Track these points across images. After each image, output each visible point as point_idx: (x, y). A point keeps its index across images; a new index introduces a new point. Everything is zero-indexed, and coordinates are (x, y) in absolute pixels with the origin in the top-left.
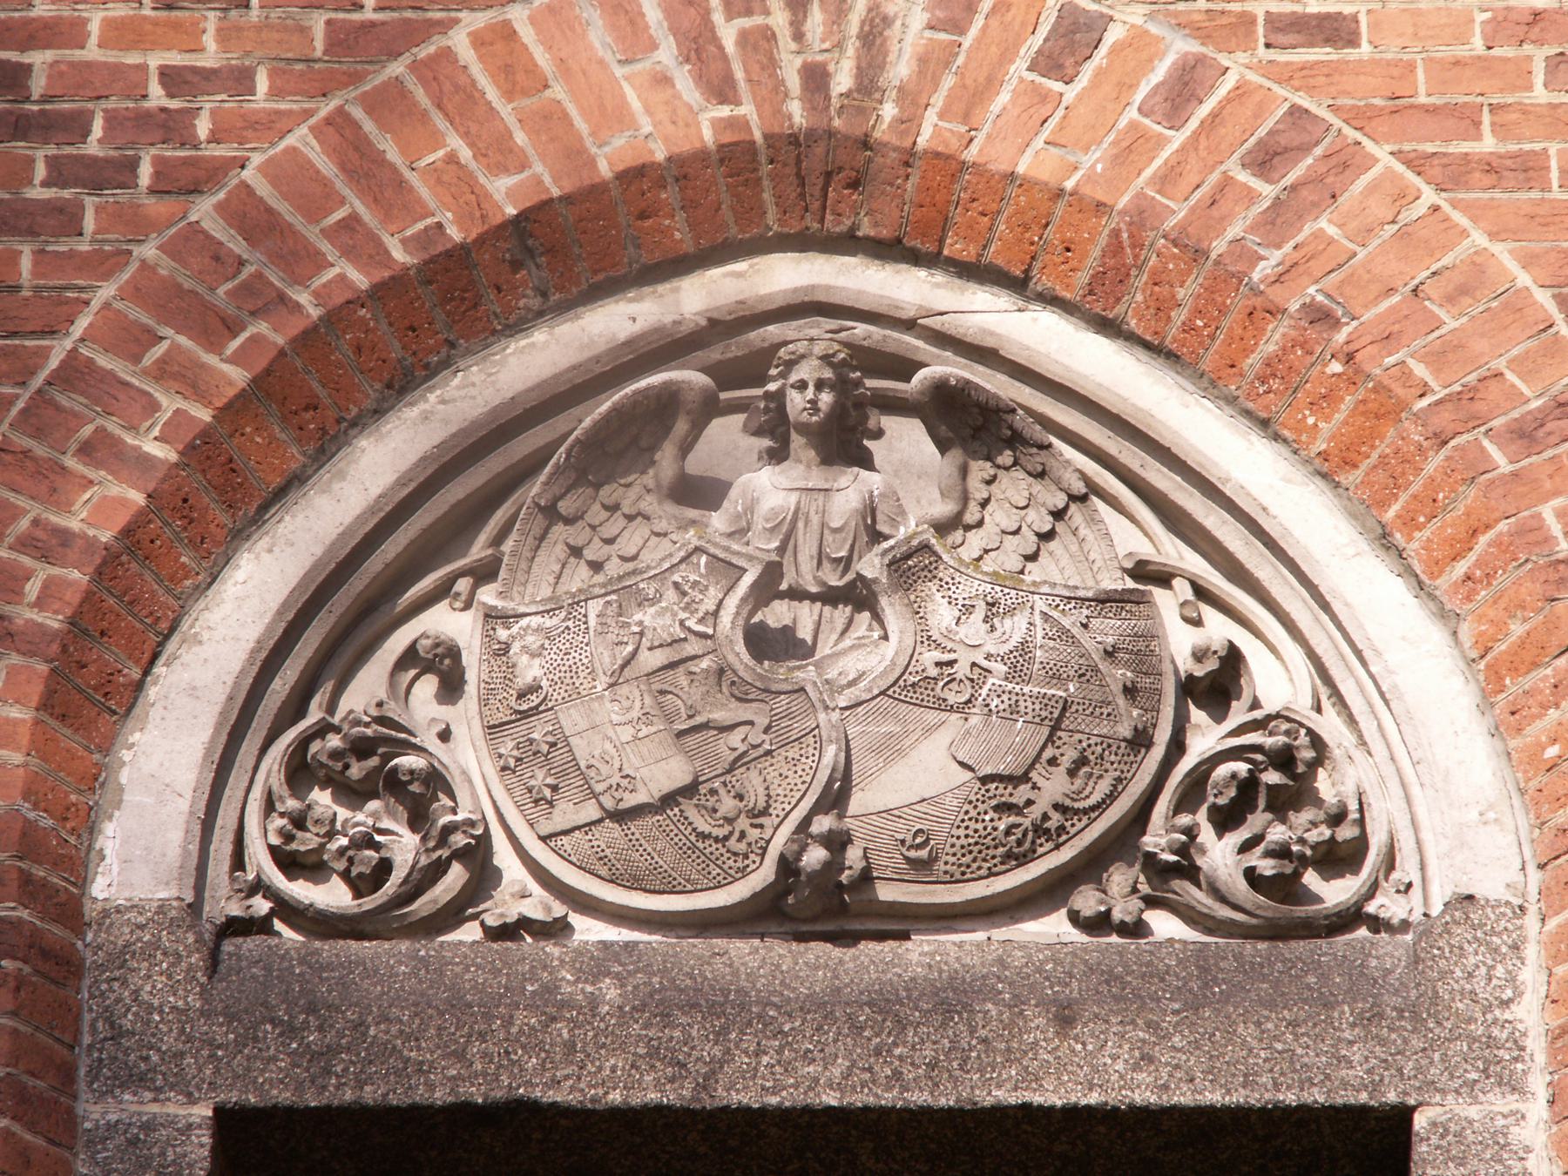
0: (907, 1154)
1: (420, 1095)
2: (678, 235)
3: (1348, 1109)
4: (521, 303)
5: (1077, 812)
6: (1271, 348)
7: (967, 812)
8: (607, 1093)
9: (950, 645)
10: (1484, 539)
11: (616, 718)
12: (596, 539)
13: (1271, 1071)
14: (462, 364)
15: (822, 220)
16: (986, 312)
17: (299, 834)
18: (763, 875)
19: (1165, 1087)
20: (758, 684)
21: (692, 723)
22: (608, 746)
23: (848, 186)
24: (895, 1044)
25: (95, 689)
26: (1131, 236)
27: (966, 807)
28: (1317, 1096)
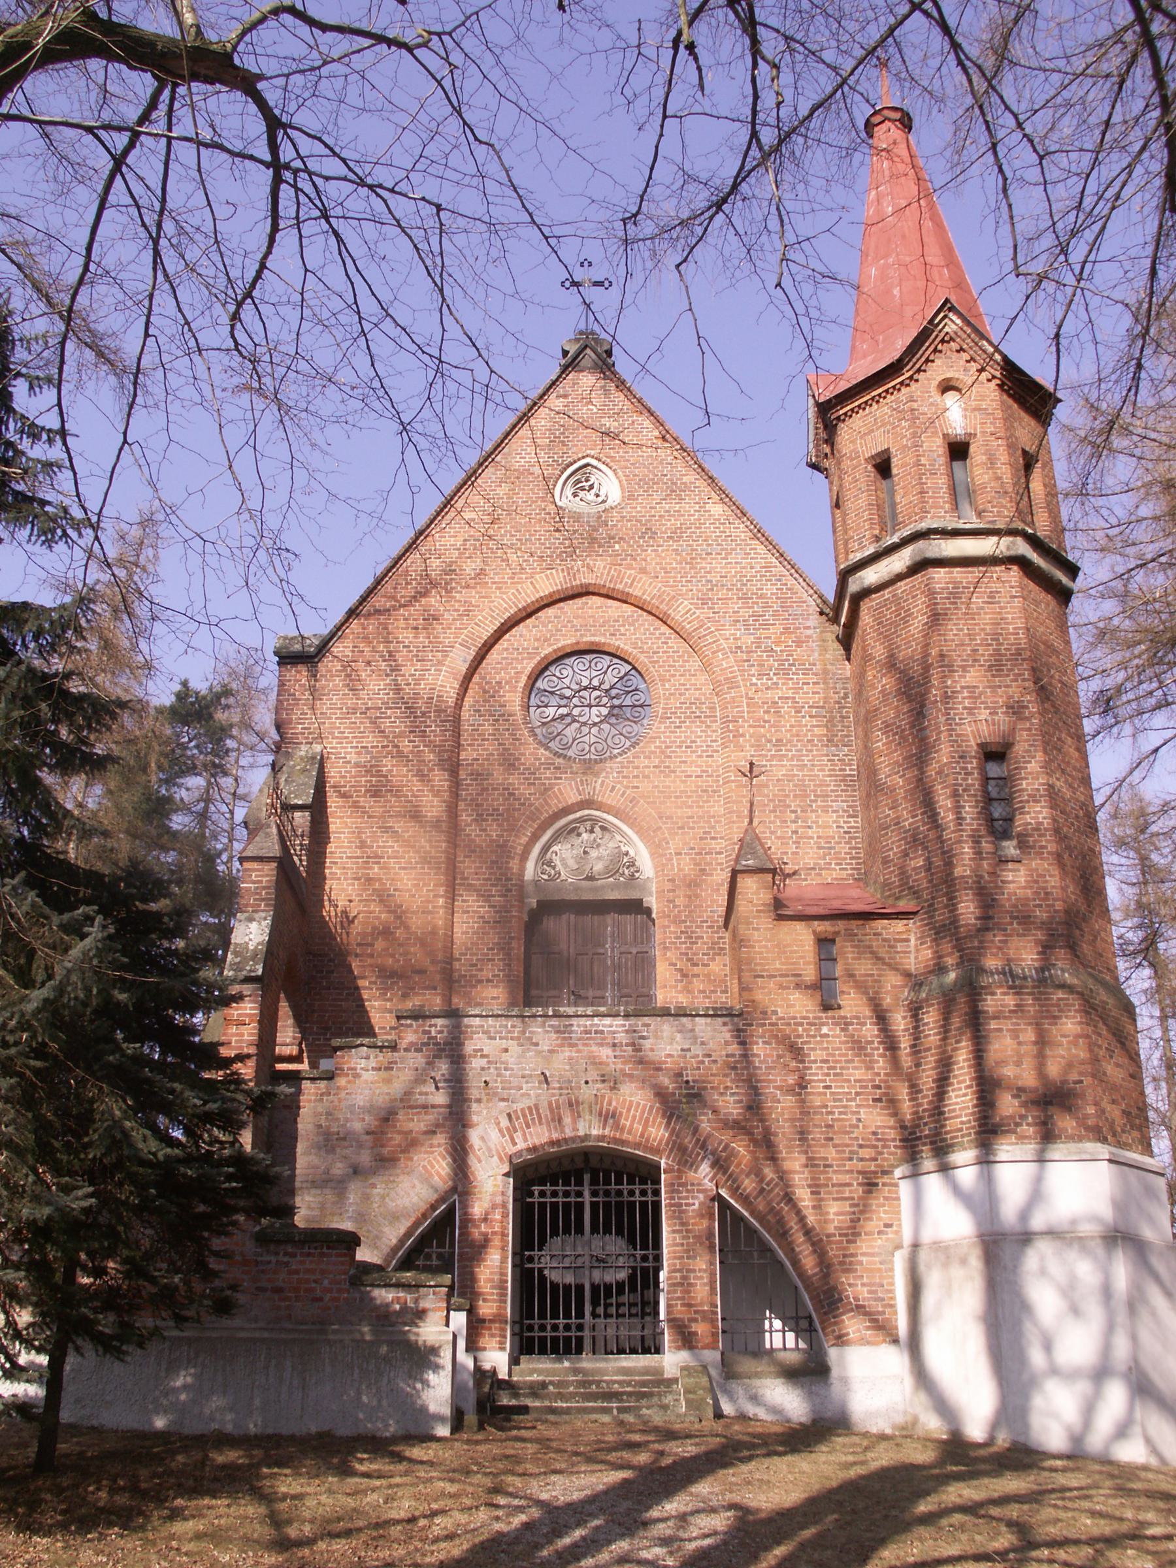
12: (412, 126)
16: (605, 816)
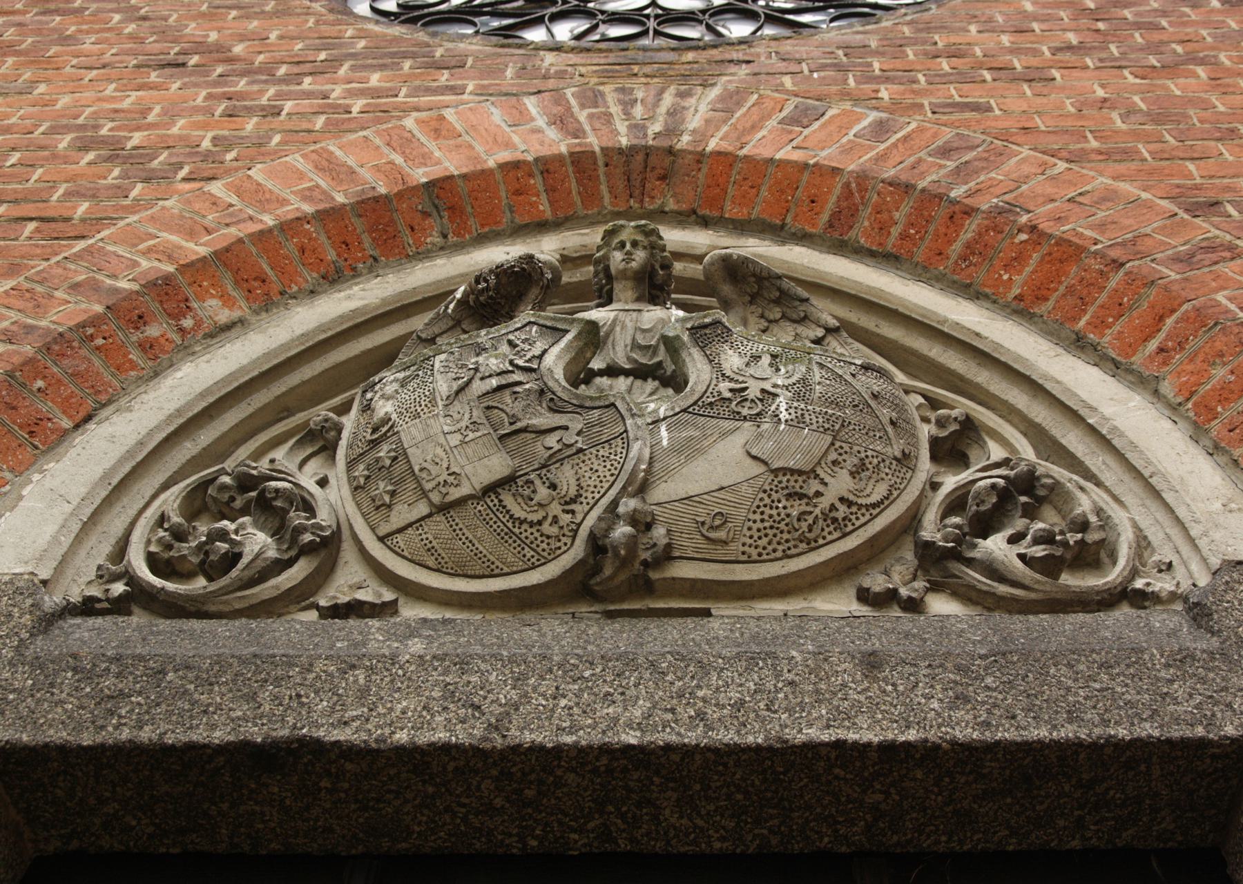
0: (712, 807)
1: (198, 735)
2: (541, 208)
3: (1184, 743)
4: (428, 240)
5: (860, 506)
6: (969, 235)
7: (761, 499)
8: (394, 733)
9: (741, 379)
10: (1169, 321)
11: (446, 429)
13: (1095, 707)
14: (381, 272)
15: (642, 201)
17: (177, 545)
18: (576, 552)
19: (987, 724)
20: (575, 402)
21: (514, 427)
22: (439, 451)
23: (659, 179)
24: (699, 687)
25: (21, 427)
26: (858, 184)
27: (761, 495)
28: (1149, 730)
